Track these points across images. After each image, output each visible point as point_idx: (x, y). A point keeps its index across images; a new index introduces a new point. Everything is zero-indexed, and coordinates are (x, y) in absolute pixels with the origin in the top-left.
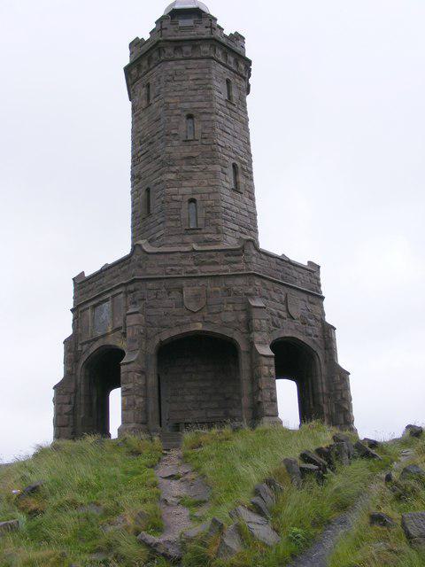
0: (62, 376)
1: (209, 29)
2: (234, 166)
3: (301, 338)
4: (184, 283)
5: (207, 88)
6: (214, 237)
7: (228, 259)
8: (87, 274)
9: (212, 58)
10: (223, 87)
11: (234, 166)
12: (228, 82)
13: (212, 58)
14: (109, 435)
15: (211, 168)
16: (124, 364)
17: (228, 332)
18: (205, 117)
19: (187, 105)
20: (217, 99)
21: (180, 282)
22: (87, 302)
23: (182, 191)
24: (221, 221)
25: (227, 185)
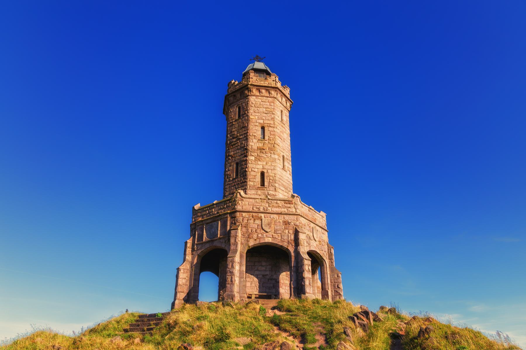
0: (281, 276)
2: (283, 156)
3: (318, 252)
4: (263, 215)
5: (271, 112)
6: (273, 193)
7: (286, 205)
9: (275, 98)
10: (279, 113)
11: (283, 156)
12: (282, 111)
13: (275, 98)
14: (402, 335)
15: (273, 156)
16: (230, 257)
17: (285, 245)
18: (271, 129)
19: (262, 121)
20: (277, 121)
21: (260, 215)
22: (211, 222)
23: (258, 167)
24: (277, 185)
25: (280, 166)
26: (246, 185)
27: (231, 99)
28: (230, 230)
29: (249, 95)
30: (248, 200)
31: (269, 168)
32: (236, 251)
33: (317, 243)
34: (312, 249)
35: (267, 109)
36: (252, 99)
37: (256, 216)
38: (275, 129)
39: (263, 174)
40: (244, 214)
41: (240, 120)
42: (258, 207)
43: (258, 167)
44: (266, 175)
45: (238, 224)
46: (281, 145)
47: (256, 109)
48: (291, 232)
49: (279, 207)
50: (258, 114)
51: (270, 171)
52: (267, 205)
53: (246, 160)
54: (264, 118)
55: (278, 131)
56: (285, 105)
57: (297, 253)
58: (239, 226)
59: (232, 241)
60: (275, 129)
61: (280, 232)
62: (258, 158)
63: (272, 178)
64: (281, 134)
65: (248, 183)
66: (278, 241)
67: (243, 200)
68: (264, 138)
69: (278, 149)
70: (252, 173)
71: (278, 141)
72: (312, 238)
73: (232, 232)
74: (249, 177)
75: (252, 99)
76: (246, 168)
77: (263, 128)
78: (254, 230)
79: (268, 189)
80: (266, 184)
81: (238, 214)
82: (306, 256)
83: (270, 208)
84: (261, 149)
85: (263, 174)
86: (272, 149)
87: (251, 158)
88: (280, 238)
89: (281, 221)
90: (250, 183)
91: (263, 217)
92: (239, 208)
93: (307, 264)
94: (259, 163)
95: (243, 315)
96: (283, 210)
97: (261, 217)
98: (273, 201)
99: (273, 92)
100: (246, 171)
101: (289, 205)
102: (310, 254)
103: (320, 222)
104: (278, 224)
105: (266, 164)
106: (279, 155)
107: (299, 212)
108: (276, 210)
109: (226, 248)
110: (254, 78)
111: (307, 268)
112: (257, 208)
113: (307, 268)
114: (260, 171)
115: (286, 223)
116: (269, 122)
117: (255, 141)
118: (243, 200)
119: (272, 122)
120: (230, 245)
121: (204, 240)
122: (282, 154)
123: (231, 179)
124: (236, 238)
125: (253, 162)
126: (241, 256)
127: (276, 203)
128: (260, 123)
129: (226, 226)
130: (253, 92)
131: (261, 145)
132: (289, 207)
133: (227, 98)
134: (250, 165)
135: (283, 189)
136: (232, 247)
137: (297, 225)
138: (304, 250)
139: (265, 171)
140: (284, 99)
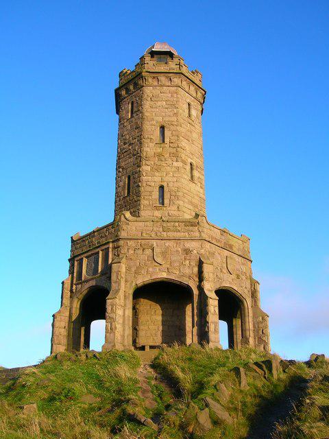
17: (185, 281)
19: (160, 119)
24: (181, 203)
26: (139, 205)
27: (123, 92)
28: (111, 264)
29: (143, 86)
32: (117, 291)
33: (233, 276)
34: (226, 284)
35: (168, 103)
36: (148, 91)
38: (178, 128)
39: (162, 187)
41: (133, 119)
43: (156, 179)
46: (187, 148)
47: (152, 103)
48: (193, 263)
52: (161, 229)
53: (139, 171)
55: (184, 130)
56: (194, 95)
57: (200, 288)
59: (114, 277)
60: (178, 128)
63: (174, 194)
65: (142, 202)
66: (174, 276)
67: (128, 224)
68: (164, 142)
70: (149, 189)
71: (184, 143)
72: (225, 271)
73: (114, 266)
76: (140, 181)
77: (162, 128)
80: (166, 201)
81: (121, 243)
82: (213, 295)
83: (165, 233)
84: (160, 155)
85: (162, 187)
87: (145, 168)
90: (144, 202)
91: (155, 245)
92: (123, 234)
93: (213, 305)
94: (157, 174)
95: (90, 375)
98: (169, 224)
99: (176, 80)
100: (138, 186)
102: (218, 292)
106: (184, 162)
107: (204, 236)
108: (171, 234)
109: (108, 289)
110: (151, 63)
114: (158, 184)
115: (187, 251)
118: (128, 224)
119: (174, 119)
120: (110, 283)
121: (83, 279)
122: (190, 160)
123: (122, 197)
124: (117, 274)
125: (149, 174)
129: (108, 260)
130: (148, 81)
131: (160, 150)
133: (117, 92)
134: (144, 178)
135: (192, 208)
136: (114, 286)
138: (210, 288)
139: (165, 184)
140: (192, 88)
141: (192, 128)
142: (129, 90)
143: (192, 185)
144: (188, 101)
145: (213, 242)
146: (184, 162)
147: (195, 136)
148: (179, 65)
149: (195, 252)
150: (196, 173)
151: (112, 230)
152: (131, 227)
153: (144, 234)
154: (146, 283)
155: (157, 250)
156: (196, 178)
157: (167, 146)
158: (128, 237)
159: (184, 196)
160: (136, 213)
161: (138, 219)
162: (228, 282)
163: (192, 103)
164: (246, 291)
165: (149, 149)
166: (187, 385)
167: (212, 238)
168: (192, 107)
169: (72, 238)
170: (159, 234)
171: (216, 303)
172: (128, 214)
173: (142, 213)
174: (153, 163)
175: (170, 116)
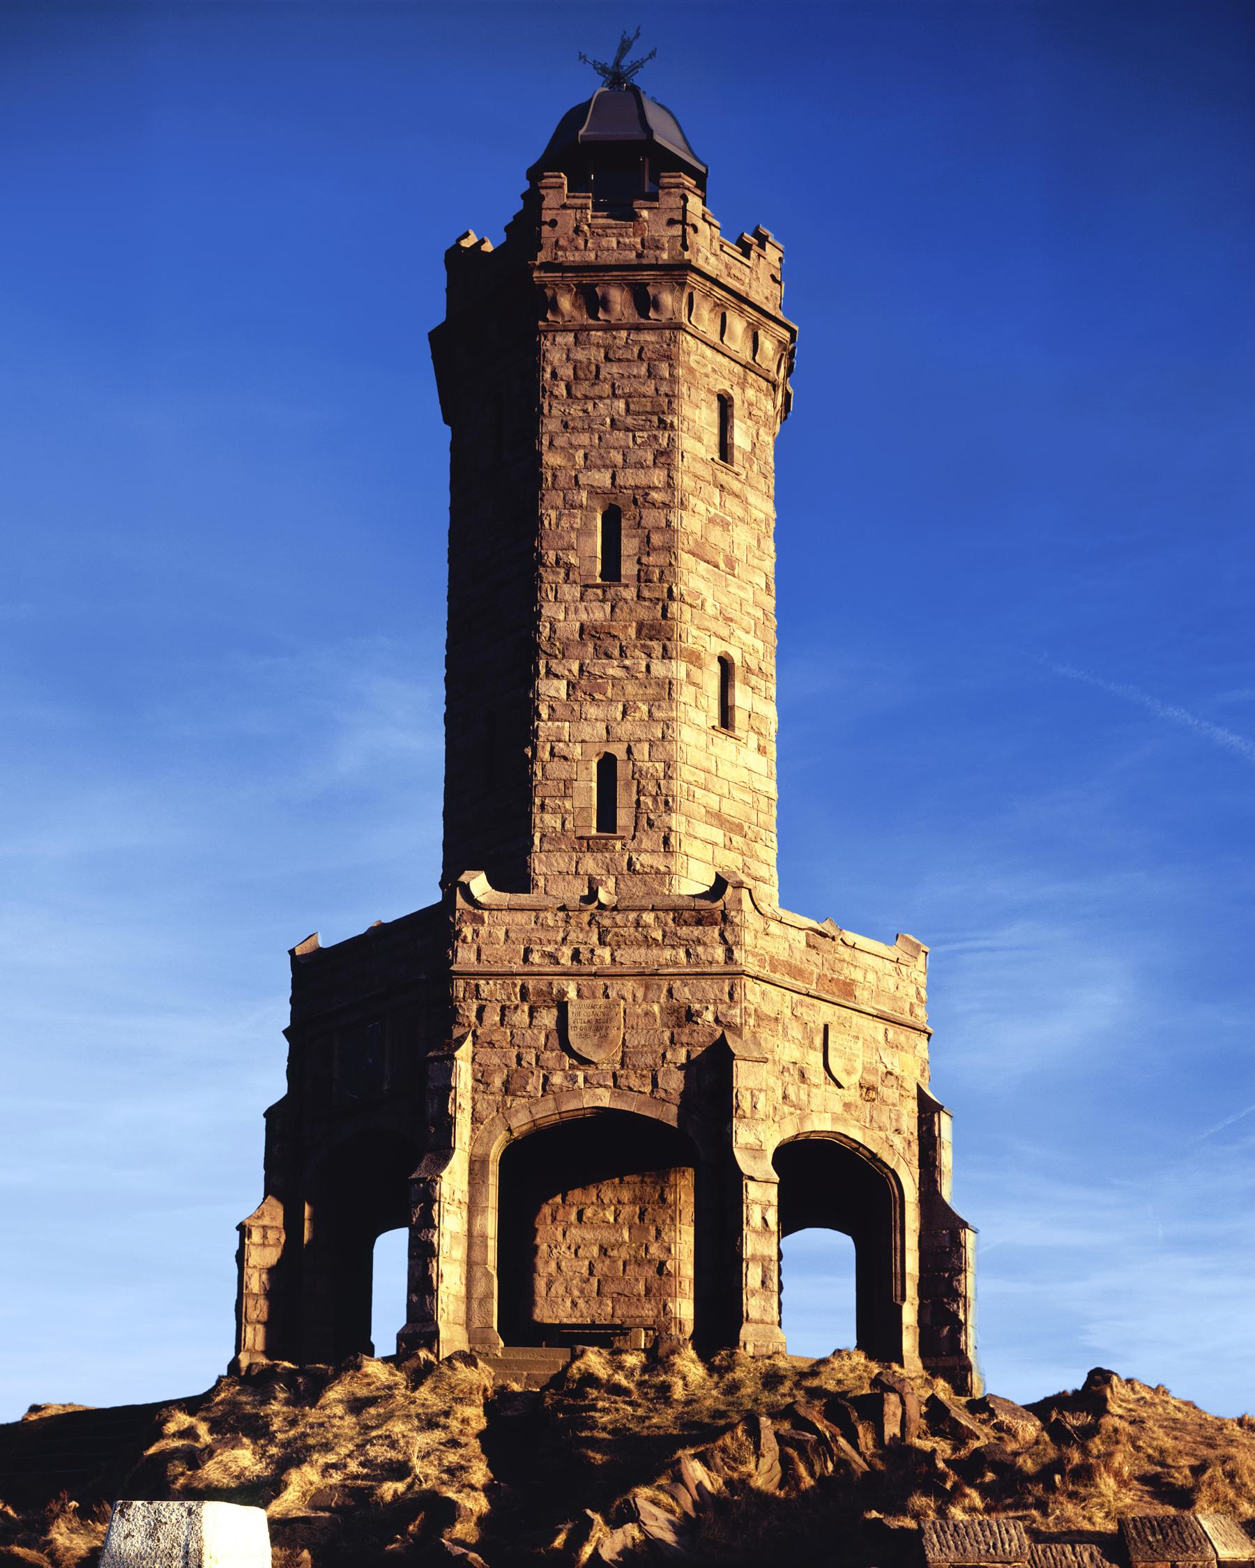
1: (677, 230)
2: (726, 665)
6: (659, 862)
8: (324, 942)
10: (704, 417)
11: (726, 665)
12: (725, 404)
15: (659, 669)
19: (602, 479)
21: (558, 983)
23: (587, 731)
30: (506, 917)
31: (640, 733)
33: (853, 1095)
37: (539, 993)
39: (607, 765)
40: (486, 987)
42: (549, 949)
43: (587, 731)
44: (623, 771)
45: (457, 1032)
49: (648, 942)
50: (584, 439)
51: (642, 751)
54: (618, 458)
58: (460, 1042)
61: (650, 1061)
62: (584, 687)
64: (716, 535)
69: (693, 632)
70: (557, 769)
74: (540, 791)
75: (557, 353)
78: (530, 1057)
79: (631, 845)
80: (624, 818)
83: (606, 953)
86: (658, 634)
88: (648, 1089)
89: (656, 1008)
91: (572, 994)
94: (592, 711)
96: (668, 953)
97: (563, 993)
98: (619, 918)
101: (697, 932)
103: (878, 993)
104: (642, 1022)
105: (624, 713)
111: (756, 1221)
112: (545, 955)
113: (756, 1221)
116: (640, 478)
117: (571, 592)
118: (481, 921)
119: (658, 477)
122: (717, 647)
125: (560, 711)
126: (477, 1168)
127: (638, 924)
128: (593, 491)
131: (599, 614)
132: (699, 942)
134: (545, 728)
137: (729, 1026)
141: (732, 505)
142: (493, 350)
143: (724, 746)
144: (723, 385)
145: (777, 977)
146: (695, 659)
147: (742, 536)
148: (683, 222)
149: (709, 1016)
150: (741, 697)
151: (420, 943)
152: (495, 929)
153: (535, 958)
154: (544, 1123)
155: (579, 1014)
156: (740, 718)
157: (630, 594)
158: (481, 969)
159: (691, 797)
160: (513, 876)
161: (523, 899)
162: (825, 1115)
163: (736, 394)
164: (897, 1141)
165: (563, 612)
166: (258, 1467)
167: (774, 965)
168: (738, 410)
169: (292, 952)
170: (585, 955)
171: (772, 1193)
172: (479, 884)
173: (539, 865)
174: (575, 667)
175: (640, 465)
